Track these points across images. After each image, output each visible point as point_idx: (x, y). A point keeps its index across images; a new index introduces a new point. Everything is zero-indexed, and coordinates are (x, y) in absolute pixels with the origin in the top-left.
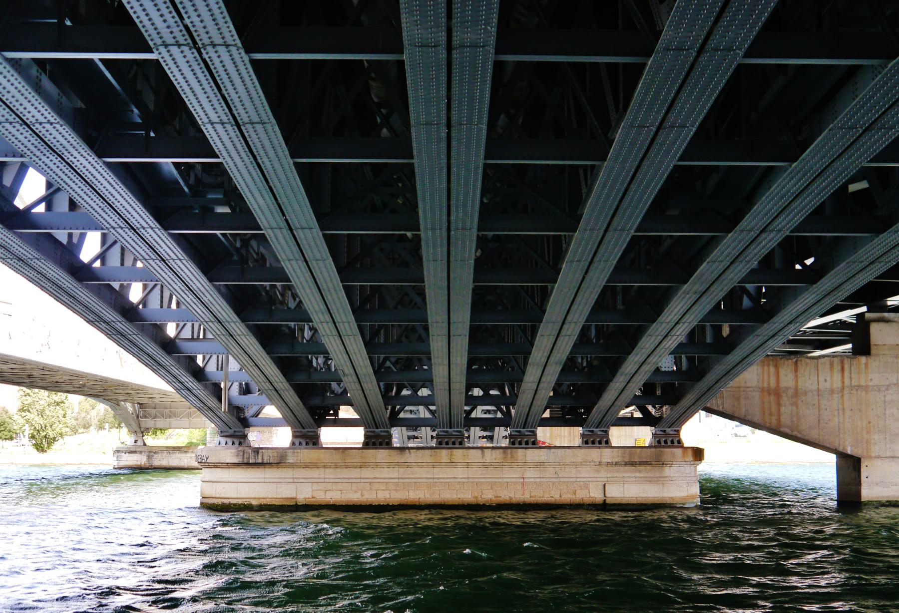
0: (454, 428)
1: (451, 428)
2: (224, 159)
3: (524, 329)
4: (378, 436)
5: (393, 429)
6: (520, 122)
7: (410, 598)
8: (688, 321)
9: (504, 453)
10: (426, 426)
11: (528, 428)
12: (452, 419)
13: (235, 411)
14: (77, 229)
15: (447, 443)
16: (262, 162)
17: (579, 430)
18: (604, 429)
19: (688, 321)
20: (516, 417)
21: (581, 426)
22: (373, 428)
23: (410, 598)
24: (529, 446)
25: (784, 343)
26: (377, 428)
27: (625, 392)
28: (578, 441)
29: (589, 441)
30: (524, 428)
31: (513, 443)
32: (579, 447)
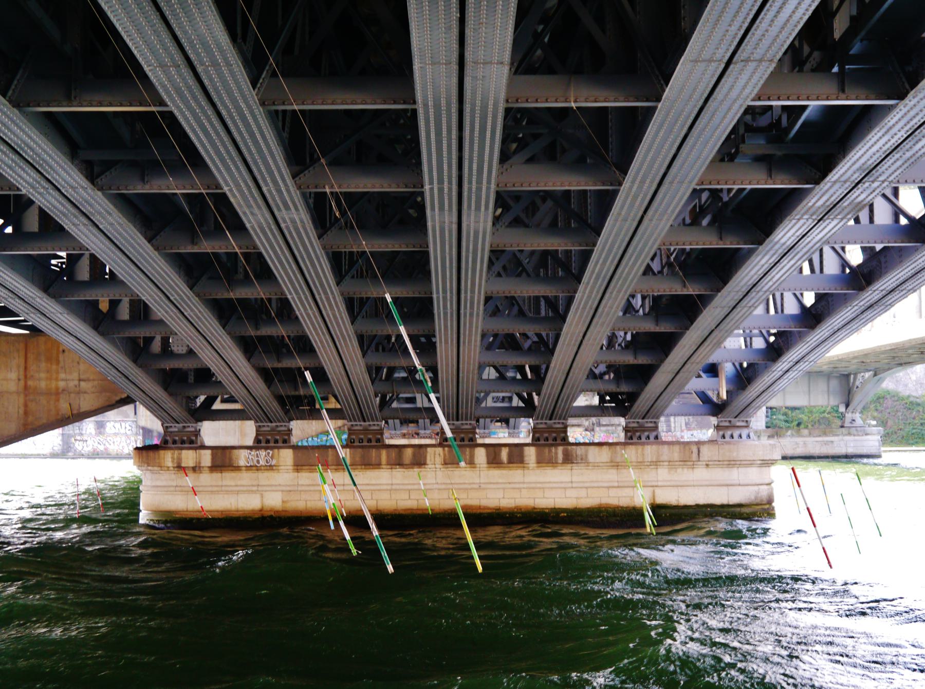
0: (462, 420)
1: (458, 420)
2: (175, 106)
3: (552, 303)
4: (550, 429)
5: (292, 423)
6: (546, 40)
7: (99, 599)
8: (735, 290)
9: (684, 447)
10: (394, 419)
11: (555, 419)
12: (557, 410)
13: (184, 401)
14: (779, 99)
15: (547, 439)
16: (739, 30)
17: (622, 421)
18: (653, 420)
19: (735, 290)
20: (541, 406)
21: (624, 416)
22: (359, 421)
23: (99, 599)
24: (372, 444)
25: (188, 346)
26: (364, 421)
27: (680, 374)
28: (621, 436)
29: (633, 435)
30: (551, 419)
31: (631, 438)
32: (250, 448)
